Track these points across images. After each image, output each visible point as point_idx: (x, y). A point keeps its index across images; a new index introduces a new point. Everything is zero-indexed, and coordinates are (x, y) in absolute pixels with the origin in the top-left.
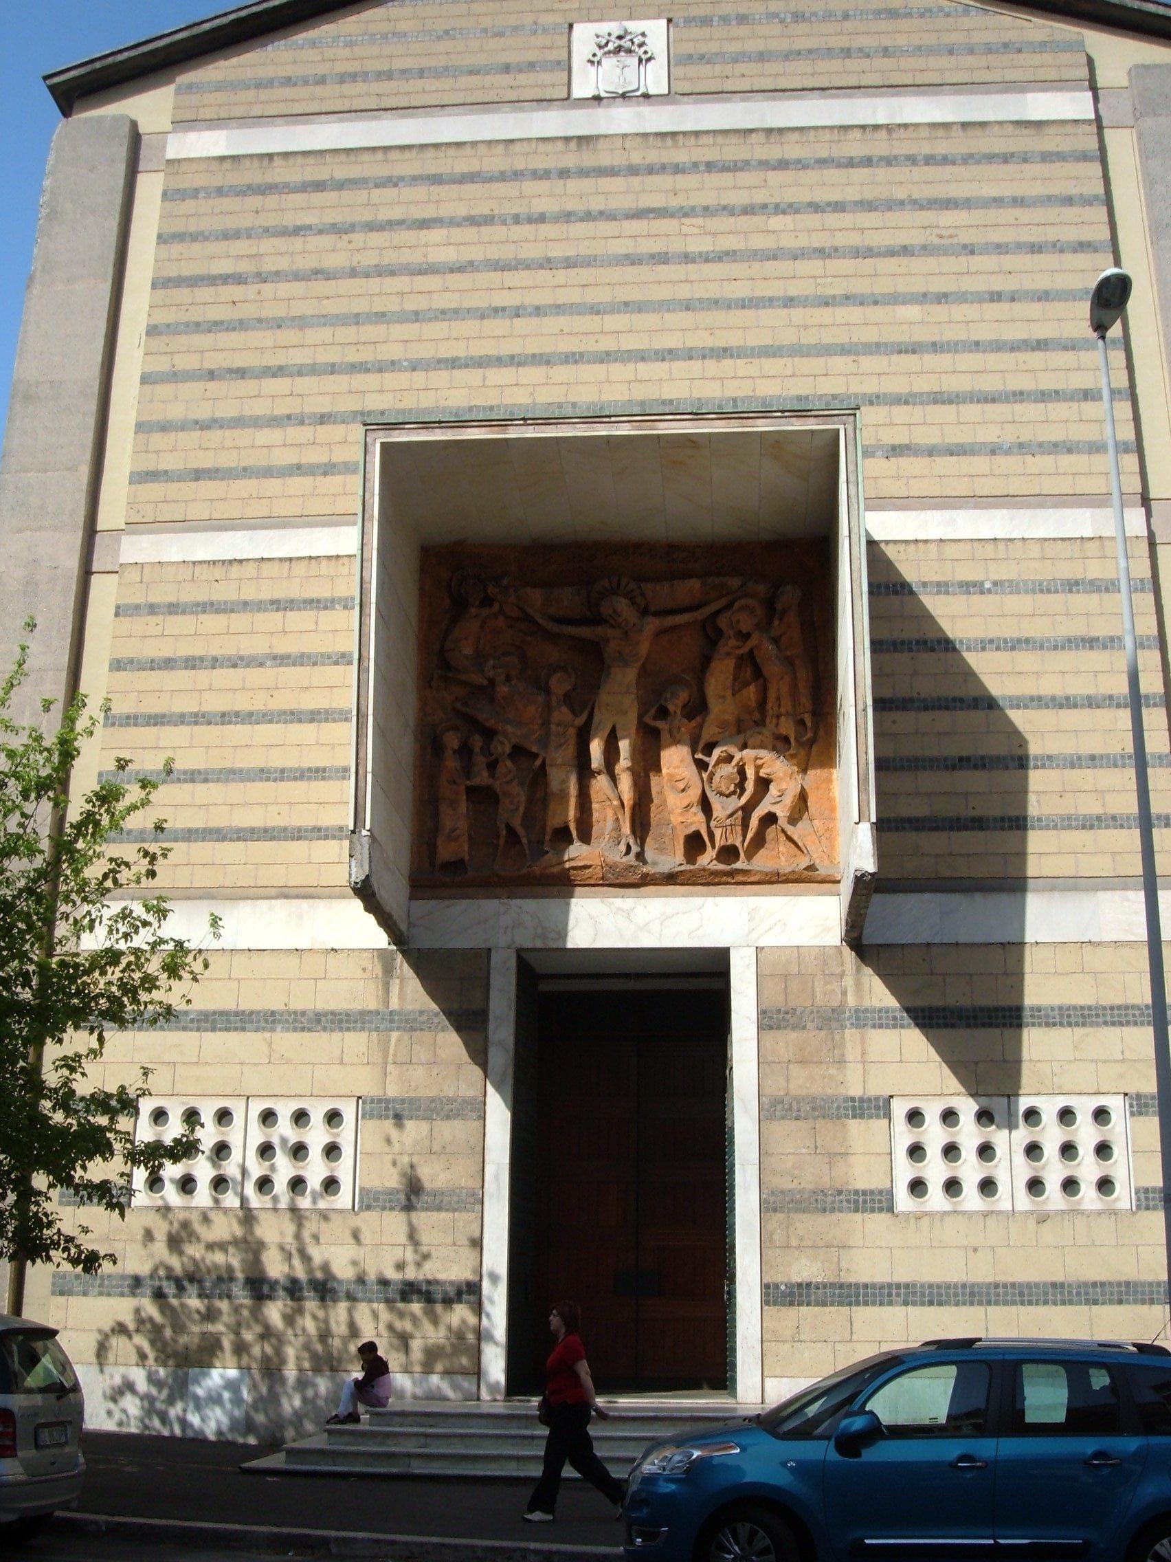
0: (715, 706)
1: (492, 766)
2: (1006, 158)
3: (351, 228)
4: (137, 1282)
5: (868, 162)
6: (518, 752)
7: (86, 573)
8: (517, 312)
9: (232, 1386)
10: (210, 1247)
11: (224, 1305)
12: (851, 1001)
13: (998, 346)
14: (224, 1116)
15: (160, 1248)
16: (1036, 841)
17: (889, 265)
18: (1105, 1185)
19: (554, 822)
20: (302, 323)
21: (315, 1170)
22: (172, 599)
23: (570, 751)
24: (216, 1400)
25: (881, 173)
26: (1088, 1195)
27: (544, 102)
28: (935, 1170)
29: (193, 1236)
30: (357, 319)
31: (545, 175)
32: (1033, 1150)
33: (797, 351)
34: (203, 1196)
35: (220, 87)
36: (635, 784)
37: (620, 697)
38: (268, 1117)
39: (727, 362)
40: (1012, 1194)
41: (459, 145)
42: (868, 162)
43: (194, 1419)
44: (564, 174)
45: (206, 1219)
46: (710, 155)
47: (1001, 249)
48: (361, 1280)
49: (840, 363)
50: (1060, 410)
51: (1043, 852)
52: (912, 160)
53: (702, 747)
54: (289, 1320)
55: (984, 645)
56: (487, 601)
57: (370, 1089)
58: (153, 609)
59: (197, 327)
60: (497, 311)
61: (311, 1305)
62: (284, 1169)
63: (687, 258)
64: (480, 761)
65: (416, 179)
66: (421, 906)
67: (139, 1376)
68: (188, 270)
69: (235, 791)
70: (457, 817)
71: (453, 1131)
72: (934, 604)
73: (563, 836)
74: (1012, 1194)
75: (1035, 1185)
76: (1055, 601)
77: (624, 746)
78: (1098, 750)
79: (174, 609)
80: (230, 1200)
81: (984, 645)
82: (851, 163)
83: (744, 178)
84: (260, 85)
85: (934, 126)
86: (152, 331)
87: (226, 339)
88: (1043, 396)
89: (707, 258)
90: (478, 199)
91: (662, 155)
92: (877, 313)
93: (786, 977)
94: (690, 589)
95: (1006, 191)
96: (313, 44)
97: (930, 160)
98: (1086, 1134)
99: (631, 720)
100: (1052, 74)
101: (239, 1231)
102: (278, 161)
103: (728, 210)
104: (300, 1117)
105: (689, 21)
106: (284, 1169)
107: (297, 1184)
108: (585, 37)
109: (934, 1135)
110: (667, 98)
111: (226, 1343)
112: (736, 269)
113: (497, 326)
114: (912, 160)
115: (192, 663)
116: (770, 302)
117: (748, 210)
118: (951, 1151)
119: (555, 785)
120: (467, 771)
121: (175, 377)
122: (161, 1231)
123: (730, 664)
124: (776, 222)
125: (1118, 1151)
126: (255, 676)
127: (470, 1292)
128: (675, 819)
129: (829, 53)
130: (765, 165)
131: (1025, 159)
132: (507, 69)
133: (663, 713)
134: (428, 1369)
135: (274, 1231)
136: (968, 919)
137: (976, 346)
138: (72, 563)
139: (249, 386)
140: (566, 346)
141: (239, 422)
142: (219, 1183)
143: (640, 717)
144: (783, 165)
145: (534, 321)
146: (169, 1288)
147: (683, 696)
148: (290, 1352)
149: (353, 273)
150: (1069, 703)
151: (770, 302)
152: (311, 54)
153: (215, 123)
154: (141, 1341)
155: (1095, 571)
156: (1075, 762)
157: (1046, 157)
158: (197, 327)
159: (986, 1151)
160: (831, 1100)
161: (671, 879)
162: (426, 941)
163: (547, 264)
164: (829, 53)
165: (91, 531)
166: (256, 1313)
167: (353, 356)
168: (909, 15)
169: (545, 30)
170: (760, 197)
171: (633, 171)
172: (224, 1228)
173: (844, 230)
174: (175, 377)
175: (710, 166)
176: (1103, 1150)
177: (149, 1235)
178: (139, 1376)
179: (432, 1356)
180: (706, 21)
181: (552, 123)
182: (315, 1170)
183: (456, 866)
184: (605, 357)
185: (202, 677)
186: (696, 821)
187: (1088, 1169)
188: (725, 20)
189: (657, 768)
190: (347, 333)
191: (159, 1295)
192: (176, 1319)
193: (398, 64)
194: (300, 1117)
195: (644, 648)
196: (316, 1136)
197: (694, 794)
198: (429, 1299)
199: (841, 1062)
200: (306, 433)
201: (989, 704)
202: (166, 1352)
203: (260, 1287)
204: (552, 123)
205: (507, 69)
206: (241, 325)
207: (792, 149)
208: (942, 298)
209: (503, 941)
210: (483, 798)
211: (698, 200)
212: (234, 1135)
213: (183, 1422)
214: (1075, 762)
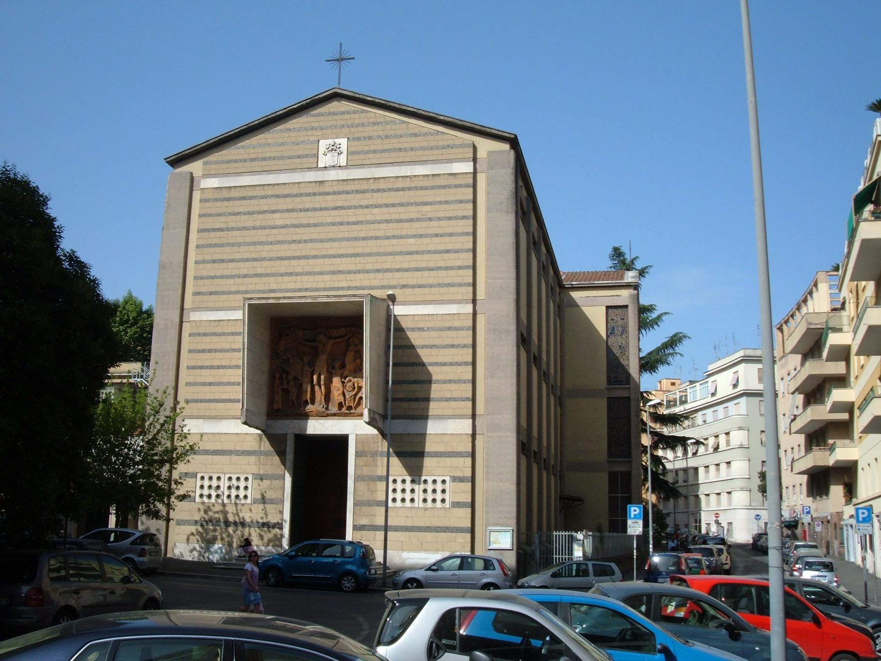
0: (348, 366)
1: (288, 382)
2: (444, 187)
3: (253, 213)
4: (196, 522)
5: (403, 189)
6: (295, 378)
7: (181, 322)
8: (300, 242)
9: (220, 549)
10: (215, 513)
11: (218, 528)
12: (380, 449)
13: (436, 252)
14: (219, 478)
15: (202, 512)
16: (432, 405)
17: (406, 225)
18: (443, 501)
19: (304, 399)
20: (239, 245)
21: (242, 493)
22: (204, 331)
23: (309, 378)
24: (216, 552)
25: (407, 193)
26: (439, 504)
27: (310, 169)
28: (399, 496)
29: (210, 510)
30: (254, 244)
31: (309, 195)
32: (425, 491)
33: (378, 254)
34: (213, 500)
35: (216, 163)
36: (326, 387)
37: (322, 363)
38: (230, 479)
39: (358, 258)
40: (419, 503)
41: (285, 184)
42: (403, 189)
43: (211, 557)
44: (315, 194)
45: (213, 505)
46: (357, 187)
47: (439, 219)
48: (252, 522)
49: (390, 258)
50: (452, 273)
51: (434, 408)
52: (416, 188)
53: (343, 377)
54: (234, 532)
55: (423, 347)
56: (287, 335)
57: (256, 472)
58: (199, 334)
59: (210, 246)
60: (294, 241)
61: (240, 528)
62: (234, 493)
63: (348, 223)
64: (285, 381)
65: (272, 196)
66: (270, 422)
67: (197, 547)
68: (207, 226)
69: (222, 388)
70: (278, 398)
71: (276, 483)
72: (410, 334)
73: (306, 403)
74: (419, 503)
75: (425, 500)
76: (444, 333)
77: (322, 377)
78: (451, 378)
79: (205, 335)
80: (220, 501)
81: (423, 347)
82: (398, 190)
83: (367, 195)
84: (228, 162)
85: (424, 176)
86: (198, 247)
87: (218, 250)
88: (447, 268)
89: (354, 223)
90: (289, 203)
91: (345, 188)
92: (402, 241)
93: (363, 442)
94: (342, 331)
95: (442, 199)
96: (243, 147)
97: (422, 188)
98: (439, 487)
99: (325, 369)
100: (461, 156)
101: (222, 508)
102: (233, 189)
103: (361, 207)
104: (238, 479)
105: (354, 139)
106: (234, 493)
107: (237, 496)
108: (324, 144)
109: (399, 486)
110: (347, 167)
111: (219, 538)
112: (362, 227)
113: (294, 246)
114: (416, 188)
115: (210, 351)
116: (371, 238)
117: (367, 207)
118: (403, 491)
119: (304, 388)
120: (282, 383)
121: (204, 262)
122: (202, 508)
123: (352, 353)
124: (375, 211)
125: (447, 492)
126: (227, 355)
127: (280, 526)
128: (336, 398)
129: (395, 150)
130: (373, 191)
131: (450, 187)
132: (299, 157)
133: (334, 368)
134: (268, 546)
135: (230, 509)
136: (411, 427)
137: (429, 252)
138: (177, 320)
139: (225, 265)
140: (314, 253)
141: (222, 277)
142: (218, 496)
143: (328, 368)
144: (378, 191)
145: (304, 245)
146: (204, 523)
147: (339, 363)
148: (235, 540)
149: (254, 228)
150: (445, 364)
151: (371, 238)
152: (242, 151)
153: (214, 176)
154: (198, 537)
155: (457, 324)
156: (445, 382)
157: (457, 186)
158: (210, 246)
159: (413, 491)
160: (373, 476)
161: (334, 415)
162: (270, 431)
163: (308, 225)
164: (395, 150)
165: (182, 309)
166: (226, 529)
167: (254, 256)
168: (420, 135)
169: (311, 143)
170: (371, 202)
171: (334, 193)
172: (218, 508)
173: (394, 213)
174: (204, 262)
175: (357, 192)
176: (444, 491)
177: (199, 510)
178: (197, 547)
179: (270, 541)
180: (359, 139)
181: (311, 176)
182: (242, 493)
183: (278, 411)
184: (324, 257)
185: (212, 355)
186: (341, 399)
187: (439, 496)
188: (365, 138)
189: (332, 382)
190: (252, 248)
191: (202, 525)
192: (206, 531)
193: (268, 155)
194: (238, 479)
195: (329, 350)
196: (242, 484)
197: (341, 391)
198: (269, 527)
199: (376, 466)
200: (240, 280)
201: (423, 364)
202: (204, 540)
203: (227, 523)
204: (311, 176)
205: (299, 157)
206: (222, 245)
207: (382, 185)
208: (421, 236)
209: (290, 431)
210: (286, 391)
211: (353, 203)
212: (221, 484)
213: (208, 558)
214: (445, 382)
